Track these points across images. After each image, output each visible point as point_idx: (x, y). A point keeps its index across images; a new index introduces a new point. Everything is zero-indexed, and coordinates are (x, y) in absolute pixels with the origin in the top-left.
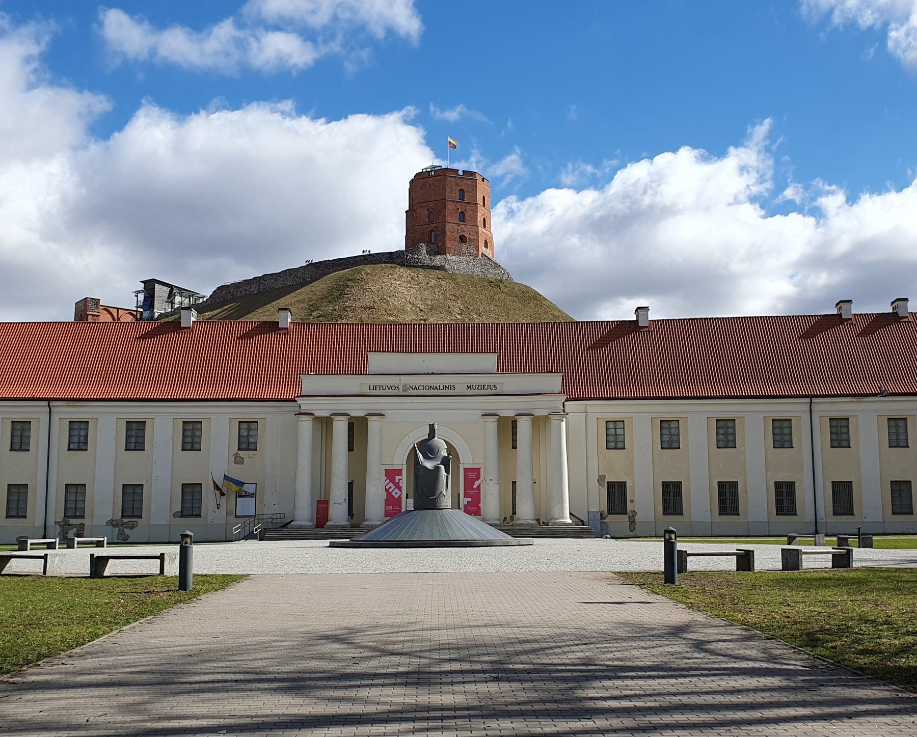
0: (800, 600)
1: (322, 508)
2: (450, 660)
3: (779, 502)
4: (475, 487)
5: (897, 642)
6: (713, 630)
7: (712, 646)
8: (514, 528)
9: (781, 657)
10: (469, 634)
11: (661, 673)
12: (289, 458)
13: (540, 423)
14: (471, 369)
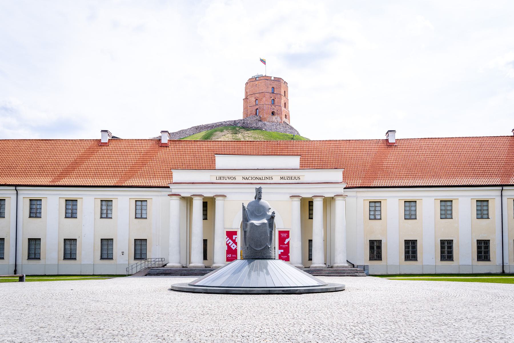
4: (286, 243)
13: (329, 202)
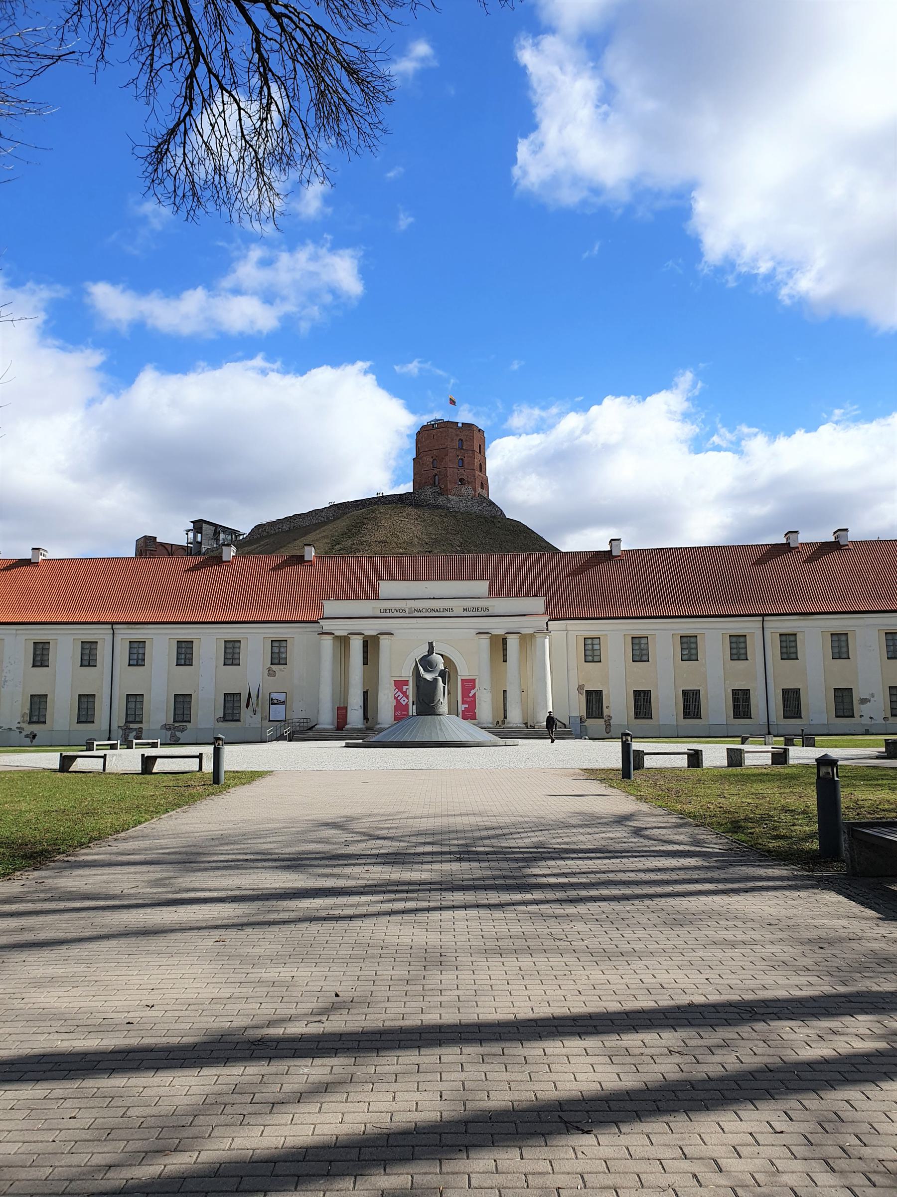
0: (735, 792)
1: (341, 713)
2: (425, 844)
3: (736, 707)
5: (807, 828)
6: (653, 817)
7: (647, 833)
8: (503, 730)
9: (704, 841)
10: (445, 821)
11: (598, 855)
12: (316, 672)
13: (526, 640)
14: (467, 594)
